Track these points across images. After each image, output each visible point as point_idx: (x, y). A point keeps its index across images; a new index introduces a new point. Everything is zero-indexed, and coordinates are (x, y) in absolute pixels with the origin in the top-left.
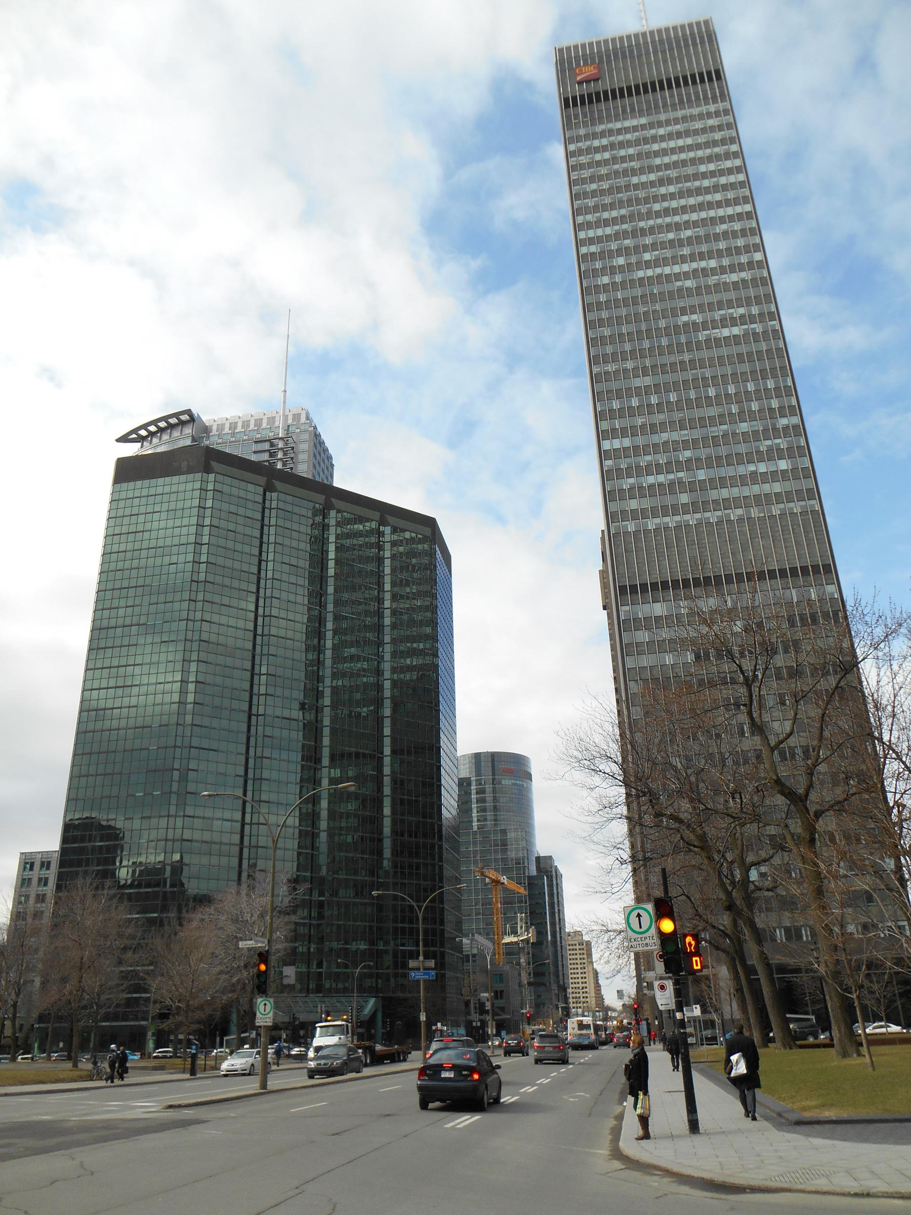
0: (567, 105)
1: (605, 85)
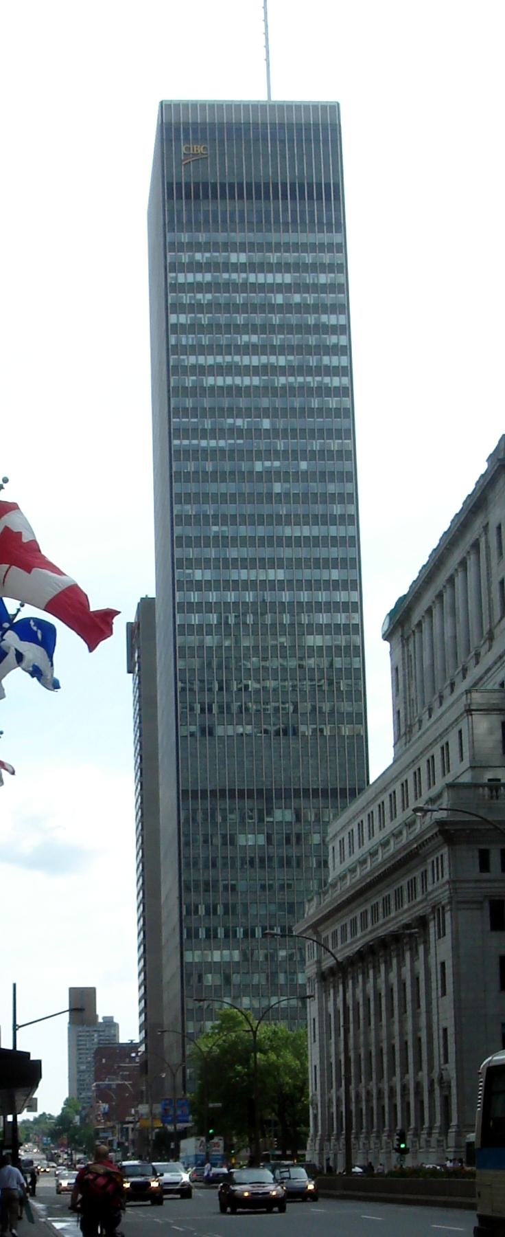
0: (170, 196)
1: (214, 176)
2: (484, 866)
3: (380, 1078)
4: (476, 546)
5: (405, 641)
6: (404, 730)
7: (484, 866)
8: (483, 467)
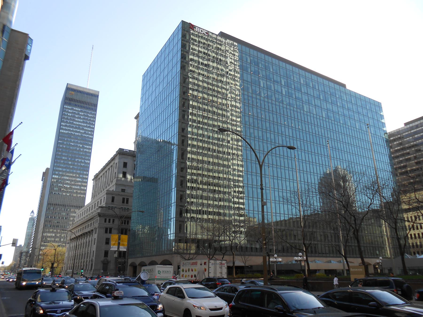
2: (105, 222)
3: (84, 258)
4: (112, 166)
5: (96, 181)
6: (93, 196)
7: (105, 222)
8: (115, 153)
